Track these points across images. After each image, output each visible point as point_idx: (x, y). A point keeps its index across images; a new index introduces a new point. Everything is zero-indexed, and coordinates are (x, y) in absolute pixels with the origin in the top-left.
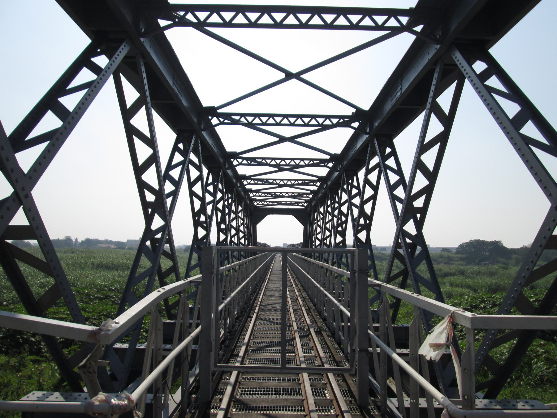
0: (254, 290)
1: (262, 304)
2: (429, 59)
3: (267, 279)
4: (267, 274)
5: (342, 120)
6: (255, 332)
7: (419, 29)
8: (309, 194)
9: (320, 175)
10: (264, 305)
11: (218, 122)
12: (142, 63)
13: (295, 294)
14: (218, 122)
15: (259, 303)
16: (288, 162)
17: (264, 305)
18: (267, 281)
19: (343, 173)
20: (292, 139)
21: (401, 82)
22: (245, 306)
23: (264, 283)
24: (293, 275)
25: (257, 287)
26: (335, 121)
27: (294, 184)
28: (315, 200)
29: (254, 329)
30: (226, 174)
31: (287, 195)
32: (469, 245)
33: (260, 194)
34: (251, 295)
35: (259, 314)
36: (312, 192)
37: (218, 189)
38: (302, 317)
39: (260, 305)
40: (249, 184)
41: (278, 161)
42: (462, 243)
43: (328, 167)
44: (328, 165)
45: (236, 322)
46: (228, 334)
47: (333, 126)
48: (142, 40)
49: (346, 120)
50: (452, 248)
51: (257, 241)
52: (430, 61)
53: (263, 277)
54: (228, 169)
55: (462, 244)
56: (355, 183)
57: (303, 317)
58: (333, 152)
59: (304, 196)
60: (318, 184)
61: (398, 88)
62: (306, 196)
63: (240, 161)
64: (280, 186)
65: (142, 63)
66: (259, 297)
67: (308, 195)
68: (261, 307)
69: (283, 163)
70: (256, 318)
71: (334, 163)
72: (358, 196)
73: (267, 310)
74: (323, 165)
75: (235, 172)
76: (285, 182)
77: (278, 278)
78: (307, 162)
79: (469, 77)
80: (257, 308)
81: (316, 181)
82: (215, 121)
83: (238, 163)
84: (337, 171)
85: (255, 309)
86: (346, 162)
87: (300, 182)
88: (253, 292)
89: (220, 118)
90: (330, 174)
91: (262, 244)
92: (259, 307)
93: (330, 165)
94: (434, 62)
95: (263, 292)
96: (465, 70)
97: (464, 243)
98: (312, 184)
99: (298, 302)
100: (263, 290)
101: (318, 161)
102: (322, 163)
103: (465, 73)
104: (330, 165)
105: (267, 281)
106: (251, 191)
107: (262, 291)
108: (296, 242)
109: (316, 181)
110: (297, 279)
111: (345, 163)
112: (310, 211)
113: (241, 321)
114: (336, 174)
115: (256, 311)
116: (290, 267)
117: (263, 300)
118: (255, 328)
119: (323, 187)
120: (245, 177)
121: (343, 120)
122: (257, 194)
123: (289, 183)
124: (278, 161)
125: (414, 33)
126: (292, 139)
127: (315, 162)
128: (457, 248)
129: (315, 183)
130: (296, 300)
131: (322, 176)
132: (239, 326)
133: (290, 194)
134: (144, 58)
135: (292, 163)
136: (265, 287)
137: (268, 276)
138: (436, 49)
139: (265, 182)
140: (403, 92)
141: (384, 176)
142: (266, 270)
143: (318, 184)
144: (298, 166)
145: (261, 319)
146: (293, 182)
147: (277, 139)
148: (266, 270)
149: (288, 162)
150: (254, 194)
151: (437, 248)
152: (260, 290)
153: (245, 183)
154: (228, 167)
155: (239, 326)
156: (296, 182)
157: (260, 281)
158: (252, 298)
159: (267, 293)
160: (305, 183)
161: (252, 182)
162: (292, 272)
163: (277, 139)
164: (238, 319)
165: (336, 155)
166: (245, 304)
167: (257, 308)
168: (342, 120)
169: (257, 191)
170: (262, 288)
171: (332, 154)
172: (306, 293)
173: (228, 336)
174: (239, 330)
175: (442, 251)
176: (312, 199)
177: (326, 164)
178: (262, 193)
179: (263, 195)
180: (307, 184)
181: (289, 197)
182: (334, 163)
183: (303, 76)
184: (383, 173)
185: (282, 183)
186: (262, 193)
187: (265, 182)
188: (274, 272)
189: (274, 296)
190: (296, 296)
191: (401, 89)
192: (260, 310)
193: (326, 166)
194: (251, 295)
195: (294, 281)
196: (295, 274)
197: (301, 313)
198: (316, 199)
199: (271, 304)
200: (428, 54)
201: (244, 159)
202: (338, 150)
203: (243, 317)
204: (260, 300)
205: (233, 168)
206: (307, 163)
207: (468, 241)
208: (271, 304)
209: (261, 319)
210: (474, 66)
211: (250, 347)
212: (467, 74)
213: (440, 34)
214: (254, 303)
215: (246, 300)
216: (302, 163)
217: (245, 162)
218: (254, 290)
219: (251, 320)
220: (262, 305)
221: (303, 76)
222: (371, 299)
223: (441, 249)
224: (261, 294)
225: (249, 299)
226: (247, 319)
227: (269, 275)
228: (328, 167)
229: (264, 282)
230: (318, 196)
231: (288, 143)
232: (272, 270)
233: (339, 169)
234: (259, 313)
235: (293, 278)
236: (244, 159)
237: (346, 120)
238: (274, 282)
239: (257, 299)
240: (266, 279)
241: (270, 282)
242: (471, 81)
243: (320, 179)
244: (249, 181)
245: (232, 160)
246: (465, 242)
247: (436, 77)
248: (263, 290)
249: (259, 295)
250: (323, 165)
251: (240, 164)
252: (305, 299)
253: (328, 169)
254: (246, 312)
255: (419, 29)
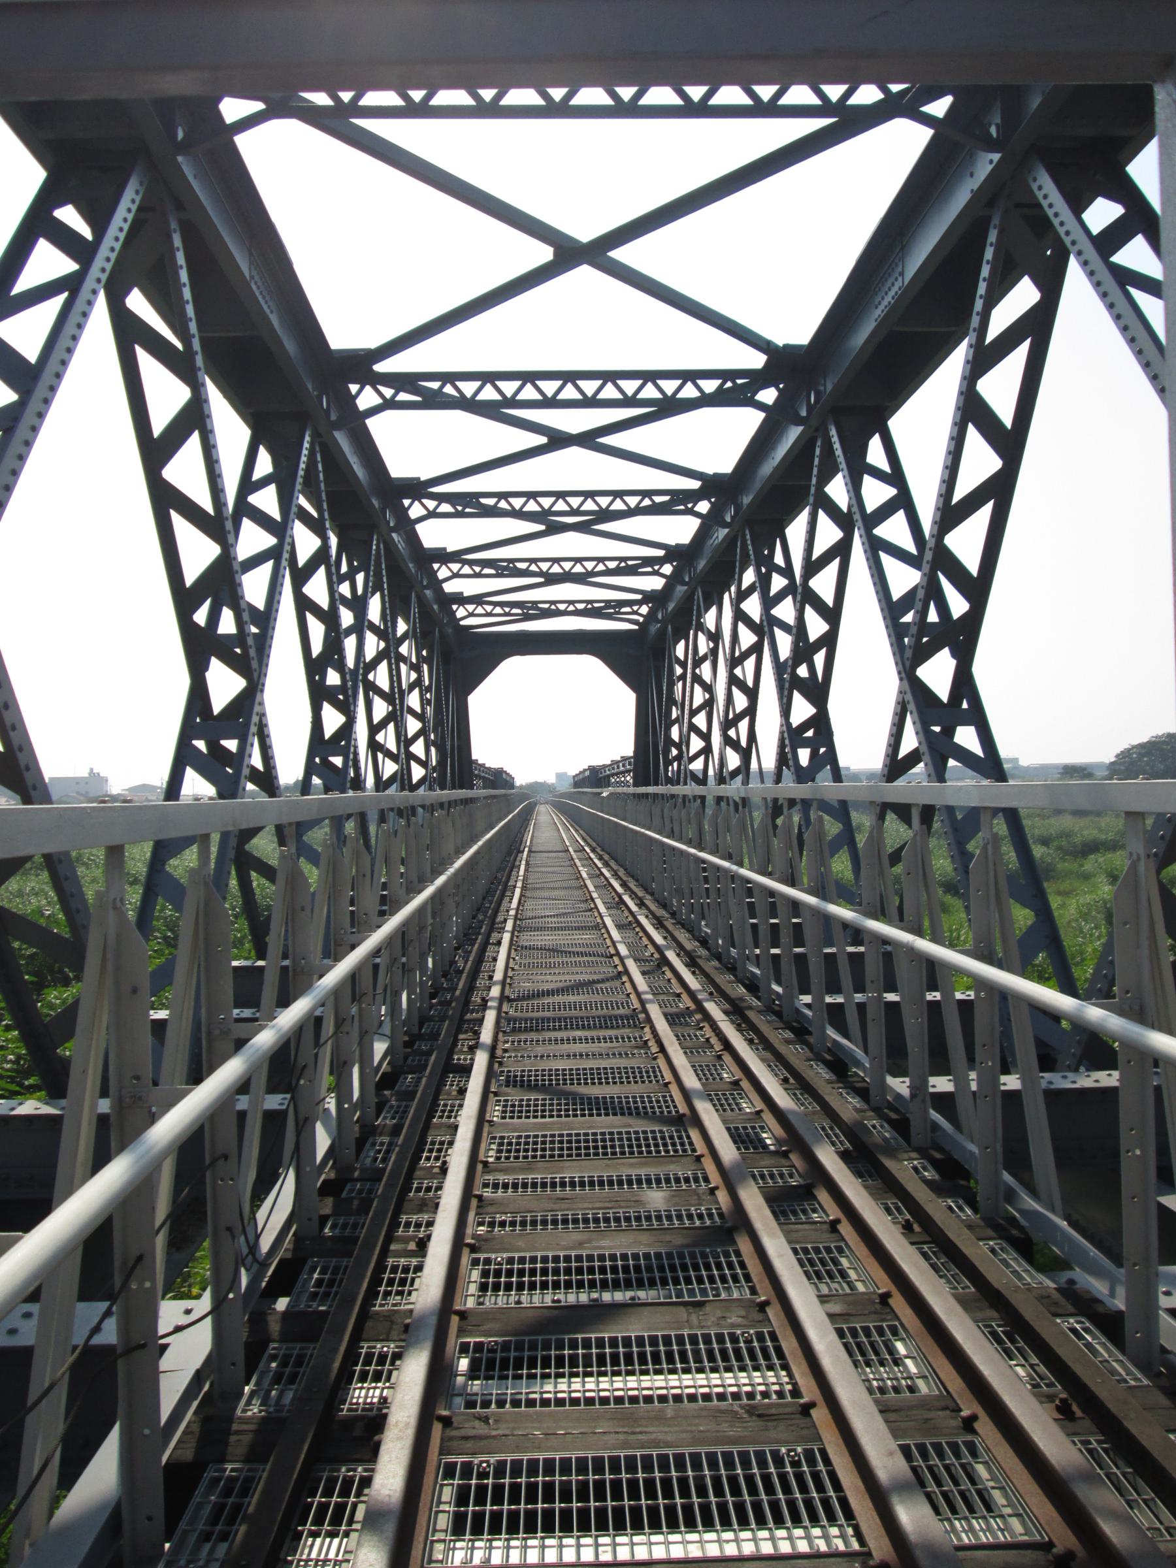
0: (470, 927)
1: (507, 992)
2: (972, 191)
3: (519, 884)
4: (514, 867)
5: (729, 384)
6: (490, 1178)
7: (939, 107)
8: (640, 603)
9: (710, 471)
10: (518, 999)
11: (379, 401)
12: (174, 225)
13: (645, 941)
14: (379, 401)
15: (495, 992)
16: (575, 502)
17: (518, 999)
18: (518, 892)
19: (696, 588)
20: (589, 440)
21: (900, 255)
22: (431, 1006)
23: (506, 899)
24: (612, 863)
25: (481, 917)
26: (710, 386)
27: (513, 402)
28: (683, 583)
29: (481, 1157)
30: (389, 546)
31: (571, 608)
32: (1148, 754)
33: (489, 608)
34: (457, 949)
35: (499, 1052)
36: (648, 597)
37: (366, 623)
38: (719, 1057)
39: (503, 998)
40: (471, 615)
41: (546, 502)
42: (1128, 746)
43: (697, 515)
44: (697, 509)
45: (380, 1107)
46: (327, 1206)
47: (706, 401)
48: (180, 159)
49: (739, 381)
50: (1099, 766)
51: (474, 757)
52: (976, 195)
53: (499, 875)
54: (339, 429)
55: (1128, 750)
56: (779, 559)
57: (727, 1058)
58: (710, 469)
59: (623, 610)
60: (667, 569)
61: (886, 280)
62: (628, 609)
63: (431, 504)
64: (551, 580)
65: (174, 225)
66: (495, 960)
67: (635, 608)
68: (505, 1008)
69: (561, 506)
70: (490, 1075)
71: (781, 386)
72: (790, 597)
73: (538, 1026)
74: (682, 507)
75: (413, 539)
76: (567, 566)
77: (556, 877)
78: (633, 501)
79: (1079, 253)
80: (490, 1017)
81: (661, 561)
82: (367, 399)
83: (450, 574)
84: (798, 421)
85: (481, 1021)
86: (750, 498)
87: (612, 565)
88: (467, 936)
89: (379, 387)
90: (701, 536)
91: (489, 769)
92: (499, 1009)
93: (703, 507)
94: (987, 198)
95: (506, 937)
96: (1067, 233)
97: (1134, 747)
98: (649, 569)
99: (669, 975)
100: (509, 926)
101: (667, 498)
102: (677, 503)
103: (1067, 241)
104: (703, 507)
105: (518, 892)
106: (461, 599)
107: (502, 930)
108: (602, 758)
109: (661, 561)
110: (630, 879)
111: (701, 564)
112: (662, 633)
113: (409, 1095)
114: (722, 533)
115: (486, 1036)
116: (595, 841)
117: (510, 973)
118: (483, 1146)
119: (798, 414)
120: (444, 556)
121: (734, 382)
122: (480, 610)
123: (578, 569)
124: (546, 502)
125: (927, 120)
126: (589, 440)
127: (658, 499)
128: (1112, 764)
129: (656, 568)
130: (659, 966)
131: (677, 545)
132: (396, 1131)
133: (581, 606)
134: (180, 206)
135: (589, 505)
136: (512, 913)
137: (522, 872)
138: (991, 162)
139: (506, 569)
140: (906, 282)
141: (861, 536)
142: (509, 853)
143: (667, 569)
144: (606, 515)
145: (512, 1081)
146: (590, 565)
147: (543, 440)
148: (509, 853)
149: (575, 502)
150: (470, 608)
151: (1043, 770)
152: (495, 926)
153: (443, 573)
154: (395, 525)
155: (396, 1131)
156: (601, 567)
157: (489, 892)
158: (461, 964)
159: (526, 939)
160: (628, 568)
161: (466, 570)
162: (606, 857)
163: (543, 440)
164: (392, 1088)
165: (790, 351)
166: (433, 996)
167: (490, 1017)
168: (729, 384)
169: (478, 600)
170: (500, 918)
171: (707, 475)
172: (689, 931)
173: (323, 1220)
174: (395, 1173)
175: (1062, 774)
176: (650, 617)
177: (690, 506)
178: (496, 604)
179: (498, 610)
180: (632, 571)
181: (578, 613)
182: (713, 500)
183: (620, 254)
184: (859, 529)
185: (556, 569)
186: (496, 604)
187: (506, 569)
188: (538, 859)
189: (554, 951)
190: (651, 949)
191: (902, 274)
192: (503, 1023)
193: (690, 512)
194: (457, 949)
195: (624, 885)
196: (616, 861)
197: (708, 1032)
198: (687, 580)
199: (550, 993)
200: (972, 175)
201: (442, 498)
202: (724, 462)
203: (420, 1069)
204: (498, 976)
205: (408, 527)
206: (632, 506)
207: (1145, 740)
208: (550, 993)
209: (512, 1081)
210: (1087, 216)
211: (461, 1332)
212: (1074, 243)
213: (998, 120)
214: (471, 988)
215: (434, 976)
216: (618, 505)
217: (446, 508)
218: (470, 927)
219: (462, 1092)
220: (509, 1000)
221: (620, 254)
222: (1022, 938)
223: (1061, 771)
224: (499, 943)
225: (448, 971)
226: (442, 1082)
227: (523, 868)
228: (697, 515)
229: (509, 893)
230: (667, 610)
231: (574, 451)
232: (530, 851)
233: (804, 413)
234: (500, 1046)
235: (616, 875)
236: (442, 498)
237: (739, 381)
238: (546, 894)
239: (486, 966)
240: (511, 883)
241: (528, 894)
242: (1084, 264)
243: (673, 553)
244: (455, 567)
245: (406, 502)
246: (1135, 742)
247: (994, 241)
248: (509, 926)
249: (490, 948)
250: (682, 507)
251: (432, 514)
252: (698, 960)
253: (760, 416)
254: (434, 1036)
255: (939, 107)
